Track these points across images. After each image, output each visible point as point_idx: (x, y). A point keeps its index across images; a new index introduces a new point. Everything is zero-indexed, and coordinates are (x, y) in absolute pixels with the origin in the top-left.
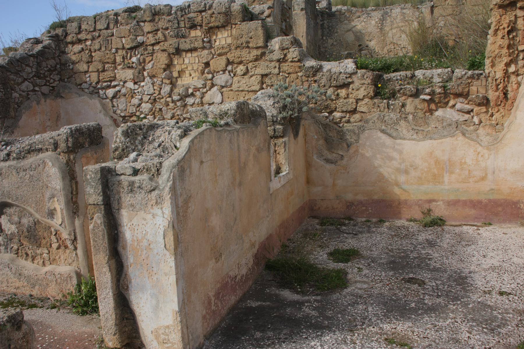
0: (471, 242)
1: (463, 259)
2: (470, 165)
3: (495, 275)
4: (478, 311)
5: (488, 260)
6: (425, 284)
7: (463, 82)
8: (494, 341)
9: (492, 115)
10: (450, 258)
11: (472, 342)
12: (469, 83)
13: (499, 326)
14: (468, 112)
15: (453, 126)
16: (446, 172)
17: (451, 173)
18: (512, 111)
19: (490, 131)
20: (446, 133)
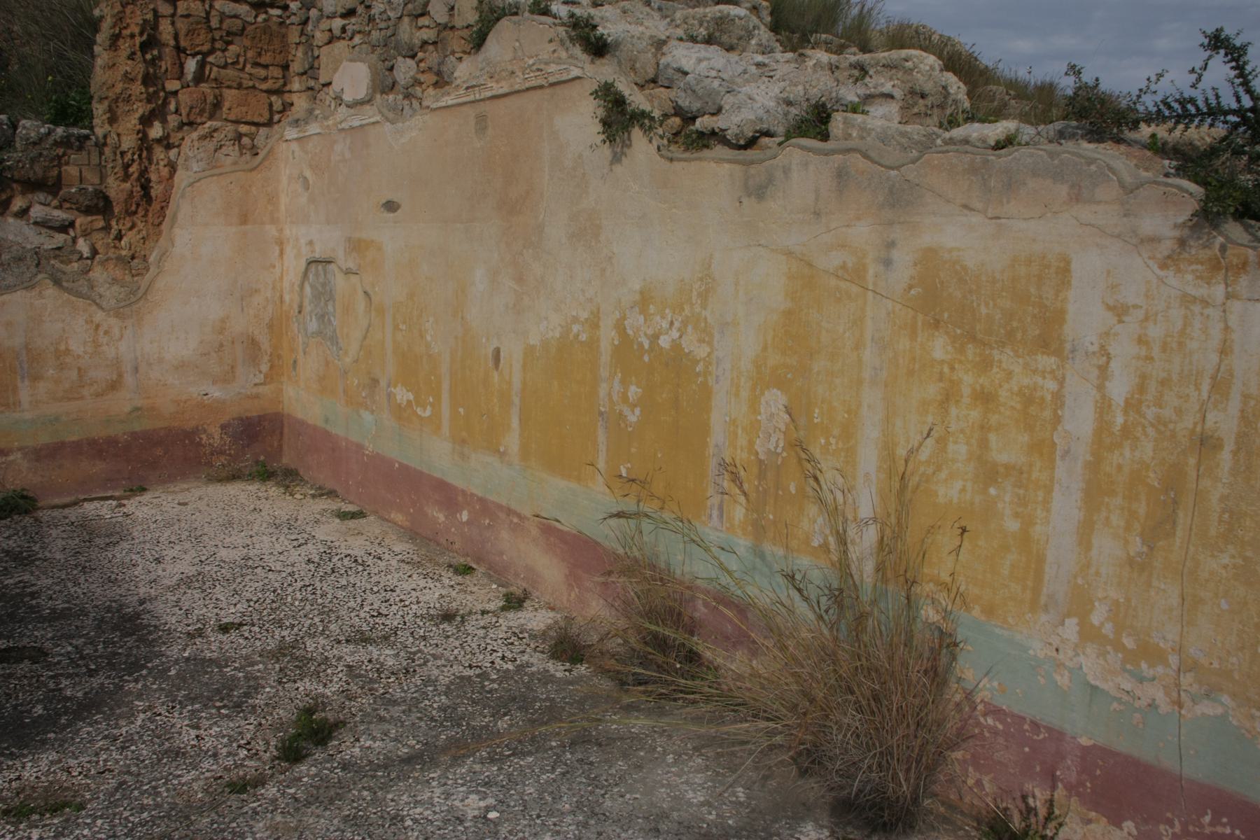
0: (116, 535)
1: (113, 576)
2: (79, 356)
3: (197, 594)
4: (192, 677)
5: (169, 568)
6: (47, 655)
7: (45, 153)
8: (251, 727)
9: (119, 237)
10: (82, 580)
11: (208, 743)
12: (59, 157)
13: (247, 695)
14: (64, 228)
15: (29, 261)
16: (23, 378)
17: (36, 378)
18: (164, 226)
19: (118, 273)
20: (10, 280)
